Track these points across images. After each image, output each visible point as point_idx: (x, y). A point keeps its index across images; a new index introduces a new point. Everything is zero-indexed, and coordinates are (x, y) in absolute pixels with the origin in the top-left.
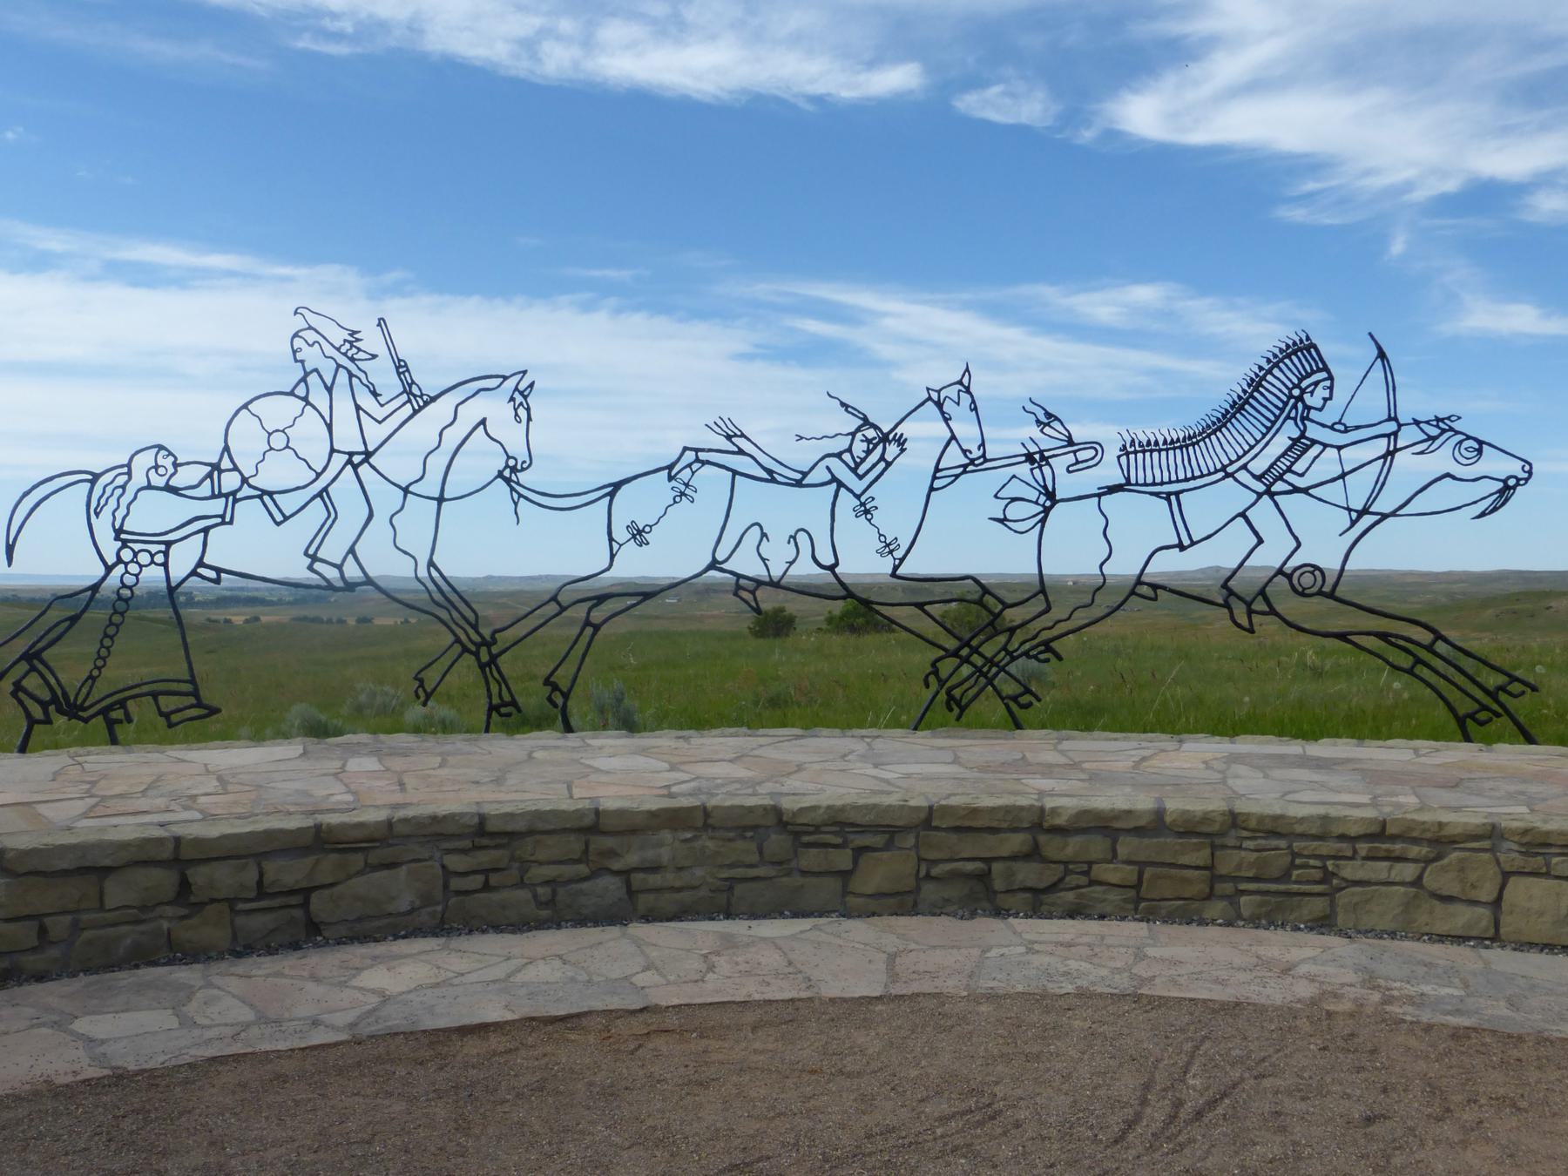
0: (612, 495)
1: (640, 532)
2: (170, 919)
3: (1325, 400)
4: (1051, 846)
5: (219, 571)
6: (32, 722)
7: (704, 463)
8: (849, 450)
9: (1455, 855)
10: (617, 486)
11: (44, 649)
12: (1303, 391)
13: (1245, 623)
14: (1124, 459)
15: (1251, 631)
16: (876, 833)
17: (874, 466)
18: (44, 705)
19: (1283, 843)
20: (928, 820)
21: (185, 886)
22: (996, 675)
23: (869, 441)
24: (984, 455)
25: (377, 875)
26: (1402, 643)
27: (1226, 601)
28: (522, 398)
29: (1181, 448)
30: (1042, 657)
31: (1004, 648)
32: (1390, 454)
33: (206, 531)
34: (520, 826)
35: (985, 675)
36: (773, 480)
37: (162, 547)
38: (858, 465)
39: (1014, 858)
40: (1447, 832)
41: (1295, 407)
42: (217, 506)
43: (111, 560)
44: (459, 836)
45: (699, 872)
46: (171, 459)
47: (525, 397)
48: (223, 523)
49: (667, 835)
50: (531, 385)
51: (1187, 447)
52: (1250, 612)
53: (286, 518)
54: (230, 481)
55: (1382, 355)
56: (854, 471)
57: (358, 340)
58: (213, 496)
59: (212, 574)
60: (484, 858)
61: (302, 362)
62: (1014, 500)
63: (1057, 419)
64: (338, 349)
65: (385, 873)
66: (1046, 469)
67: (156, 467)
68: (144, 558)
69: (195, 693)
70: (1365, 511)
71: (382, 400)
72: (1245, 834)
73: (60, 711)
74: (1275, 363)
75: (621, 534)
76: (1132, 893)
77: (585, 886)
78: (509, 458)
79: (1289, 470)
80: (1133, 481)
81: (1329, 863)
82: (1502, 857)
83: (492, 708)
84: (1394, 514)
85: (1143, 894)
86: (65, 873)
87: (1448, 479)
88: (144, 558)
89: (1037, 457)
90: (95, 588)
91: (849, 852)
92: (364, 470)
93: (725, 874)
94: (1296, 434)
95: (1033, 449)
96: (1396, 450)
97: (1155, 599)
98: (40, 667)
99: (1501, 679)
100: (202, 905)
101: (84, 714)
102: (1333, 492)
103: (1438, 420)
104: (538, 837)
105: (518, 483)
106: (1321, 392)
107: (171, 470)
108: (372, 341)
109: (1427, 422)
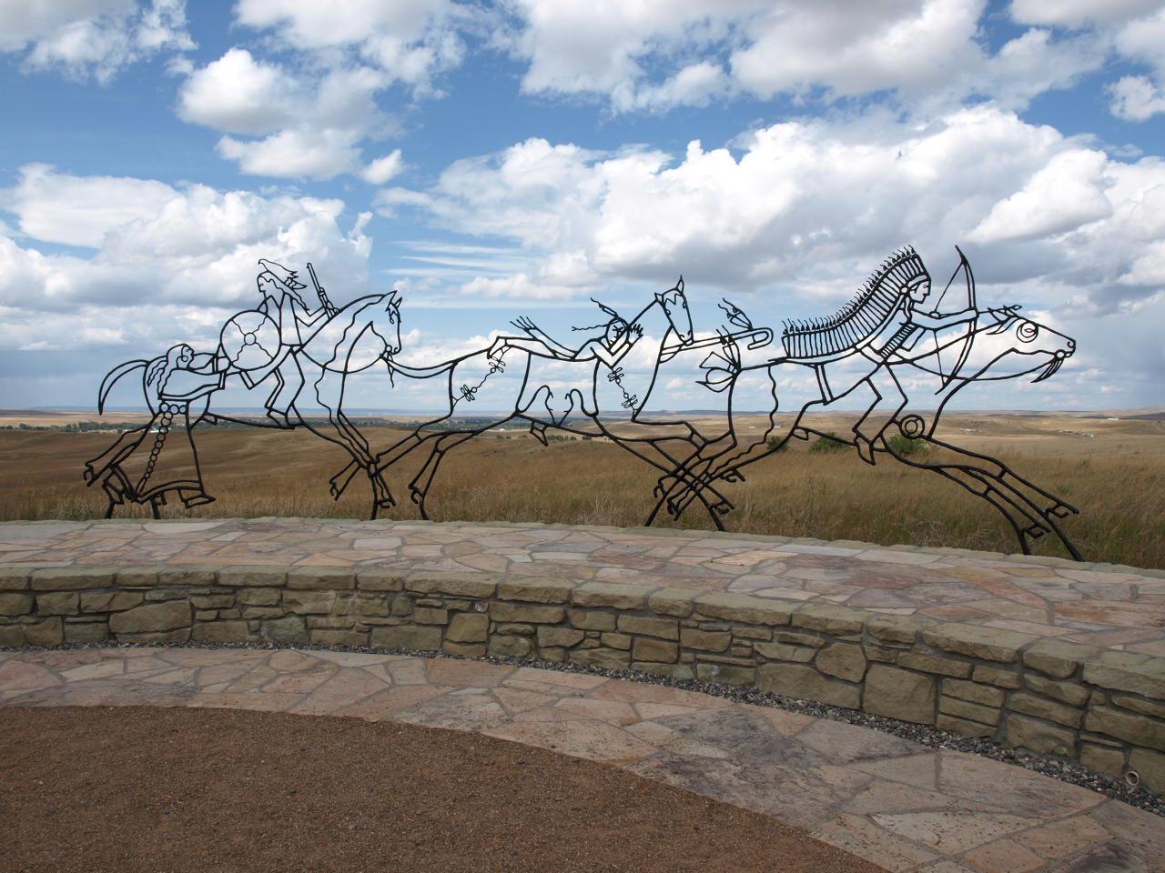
0: (452, 368)
1: (469, 392)
2: (28, 624)
3: (925, 295)
5: (217, 417)
6: (113, 503)
7: (511, 346)
8: (606, 336)
9: (836, 644)
10: (455, 362)
11: (119, 462)
12: (909, 289)
13: (869, 458)
14: (786, 339)
17: (622, 347)
18: (120, 494)
19: (725, 627)
23: (618, 330)
24: (692, 338)
25: (150, 606)
26: (979, 474)
27: (855, 440)
28: (394, 312)
29: (825, 331)
30: (731, 478)
31: (706, 471)
32: (971, 334)
33: (209, 393)
34: (238, 581)
35: (693, 488)
37: (185, 403)
38: (611, 346)
40: (830, 626)
41: (904, 300)
43: (156, 411)
44: (203, 586)
46: (190, 352)
47: (397, 308)
50: (400, 300)
51: (829, 330)
52: (872, 449)
53: (254, 385)
54: (223, 364)
55: (964, 262)
56: (608, 350)
57: (295, 277)
58: (214, 373)
59: (212, 419)
60: (217, 600)
61: (264, 292)
62: (713, 369)
63: (741, 312)
64: (284, 283)
66: (733, 347)
67: (182, 357)
68: (174, 410)
69: (201, 488)
70: (953, 376)
74: (889, 270)
75: (457, 394)
76: (626, 655)
77: (278, 622)
78: (387, 345)
80: (792, 355)
81: (756, 645)
84: (974, 378)
85: (634, 657)
87: (1013, 353)
88: (174, 410)
89: (727, 339)
91: (446, 612)
92: (300, 356)
94: (904, 320)
97: (807, 439)
99: (1051, 503)
102: (930, 362)
103: (1005, 308)
104: (251, 589)
105: (392, 361)
106: (922, 289)
107: (190, 358)
109: (998, 311)
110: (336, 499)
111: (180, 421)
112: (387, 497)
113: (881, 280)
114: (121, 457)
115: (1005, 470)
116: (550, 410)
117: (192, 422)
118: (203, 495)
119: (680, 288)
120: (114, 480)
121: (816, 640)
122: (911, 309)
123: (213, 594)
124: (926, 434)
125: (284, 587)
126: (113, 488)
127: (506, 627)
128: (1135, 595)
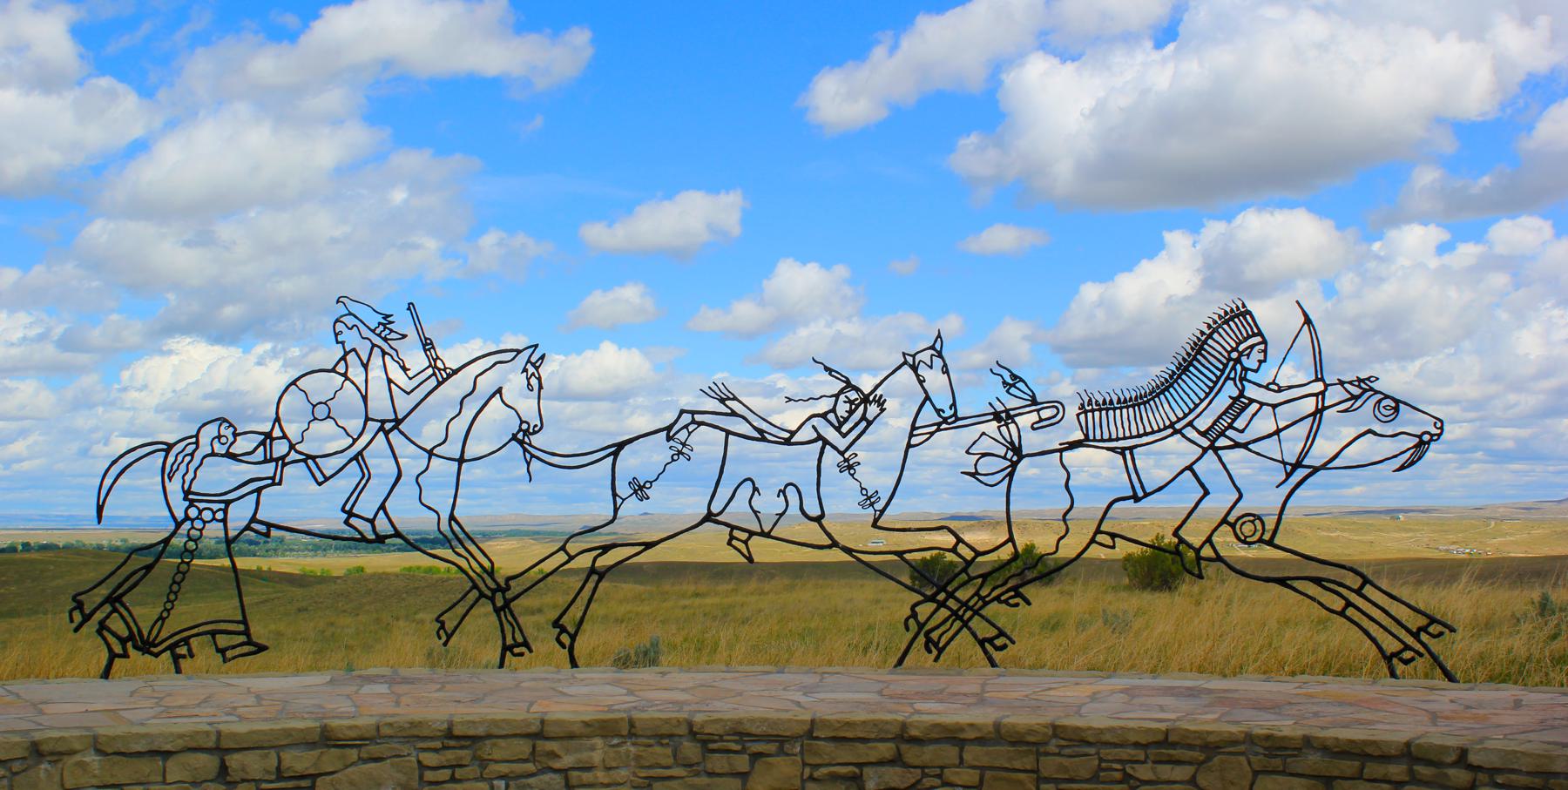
0: (616, 454)
1: (641, 488)
3: (1260, 362)
4: (912, 754)
5: (269, 526)
7: (700, 424)
8: (833, 410)
10: (621, 446)
12: (1241, 354)
14: (1082, 417)
15: (1200, 577)
16: (770, 741)
17: (857, 424)
18: (123, 641)
19: (1092, 751)
20: (810, 731)
21: (224, 769)
22: (971, 618)
23: (851, 402)
24: (955, 414)
32: (1319, 412)
33: (259, 491)
34: (481, 731)
35: (960, 618)
36: (764, 439)
38: (841, 424)
39: (880, 763)
40: (1211, 739)
41: (1234, 368)
42: (268, 470)
43: (180, 515)
44: (432, 738)
45: (624, 772)
47: (537, 368)
48: (273, 484)
49: (598, 742)
50: (542, 357)
53: (327, 479)
54: (280, 448)
55: (1308, 321)
56: (838, 429)
58: (265, 461)
59: (262, 528)
60: (450, 756)
61: (343, 343)
62: (984, 455)
63: (1022, 380)
65: (373, 765)
66: (1012, 427)
67: (219, 437)
68: (207, 515)
69: (247, 633)
70: (1298, 465)
71: (411, 374)
72: (1063, 743)
73: (135, 647)
75: (624, 490)
77: (531, 781)
78: (522, 422)
79: (1230, 426)
82: (1253, 759)
83: (506, 648)
84: (1324, 467)
86: (139, 754)
90: (166, 541)
92: (394, 436)
93: (643, 773)
94: (1235, 393)
95: (1000, 408)
96: (1325, 408)
97: (1113, 547)
98: (122, 610)
99: (1423, 621)
100: (236, 783)
101: (156, 650)
103: (1359, 380)
106: (1256, 355)
107: (231, 439)
108: (402, 323)
109: (1350, 383)
110: (445, 644)
111: (214, 530)
112: (520, 639)
113: (1205, 342)
114: (125, 587)
115: (1366, 581)
116: (755, 512)
117: (232, 534)
118: (249, 642)
119: (938, 346)
120: (116, 624)
121: (1197, 755)
122: (1242, 379)
123: (445, 748)
124: (1267, 537)
125: (539, 735)
126: (114, 634)
127: (824, 770)
128: (1518, 704)
